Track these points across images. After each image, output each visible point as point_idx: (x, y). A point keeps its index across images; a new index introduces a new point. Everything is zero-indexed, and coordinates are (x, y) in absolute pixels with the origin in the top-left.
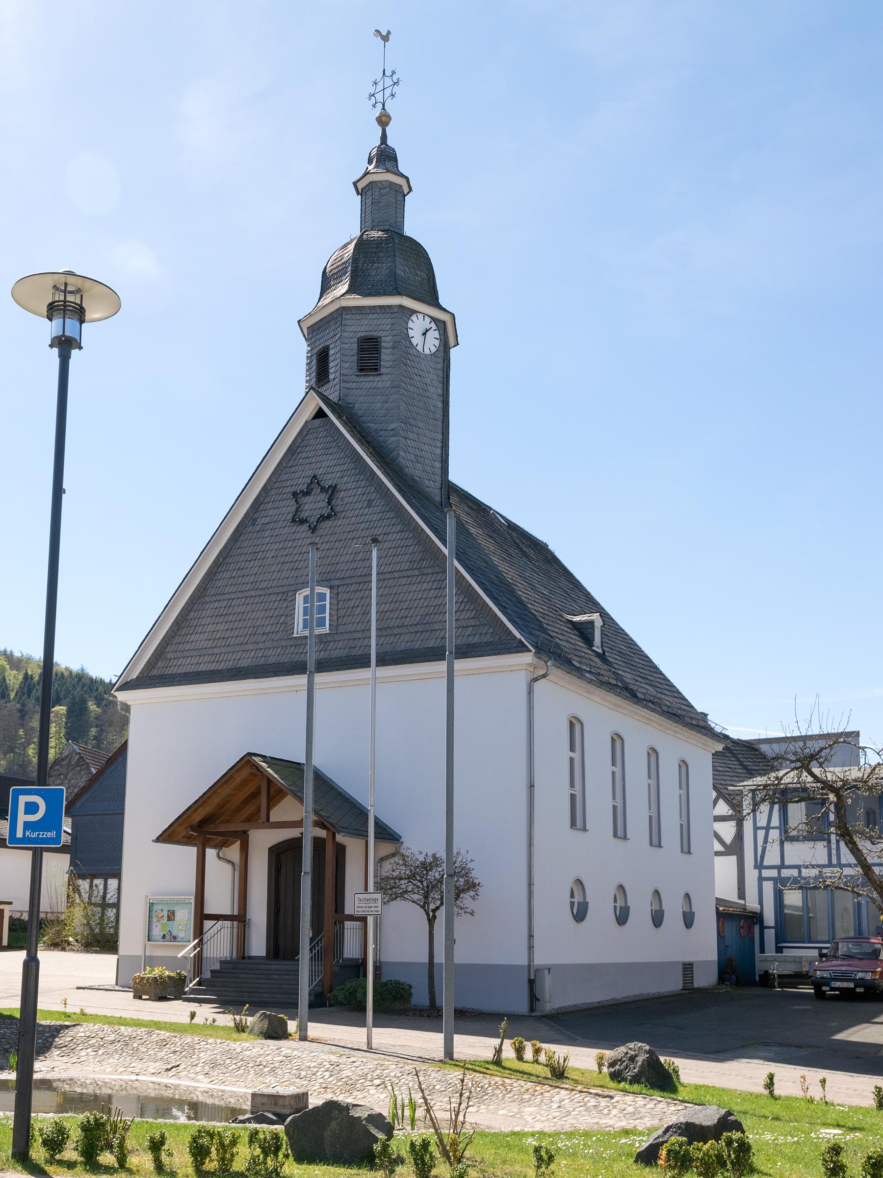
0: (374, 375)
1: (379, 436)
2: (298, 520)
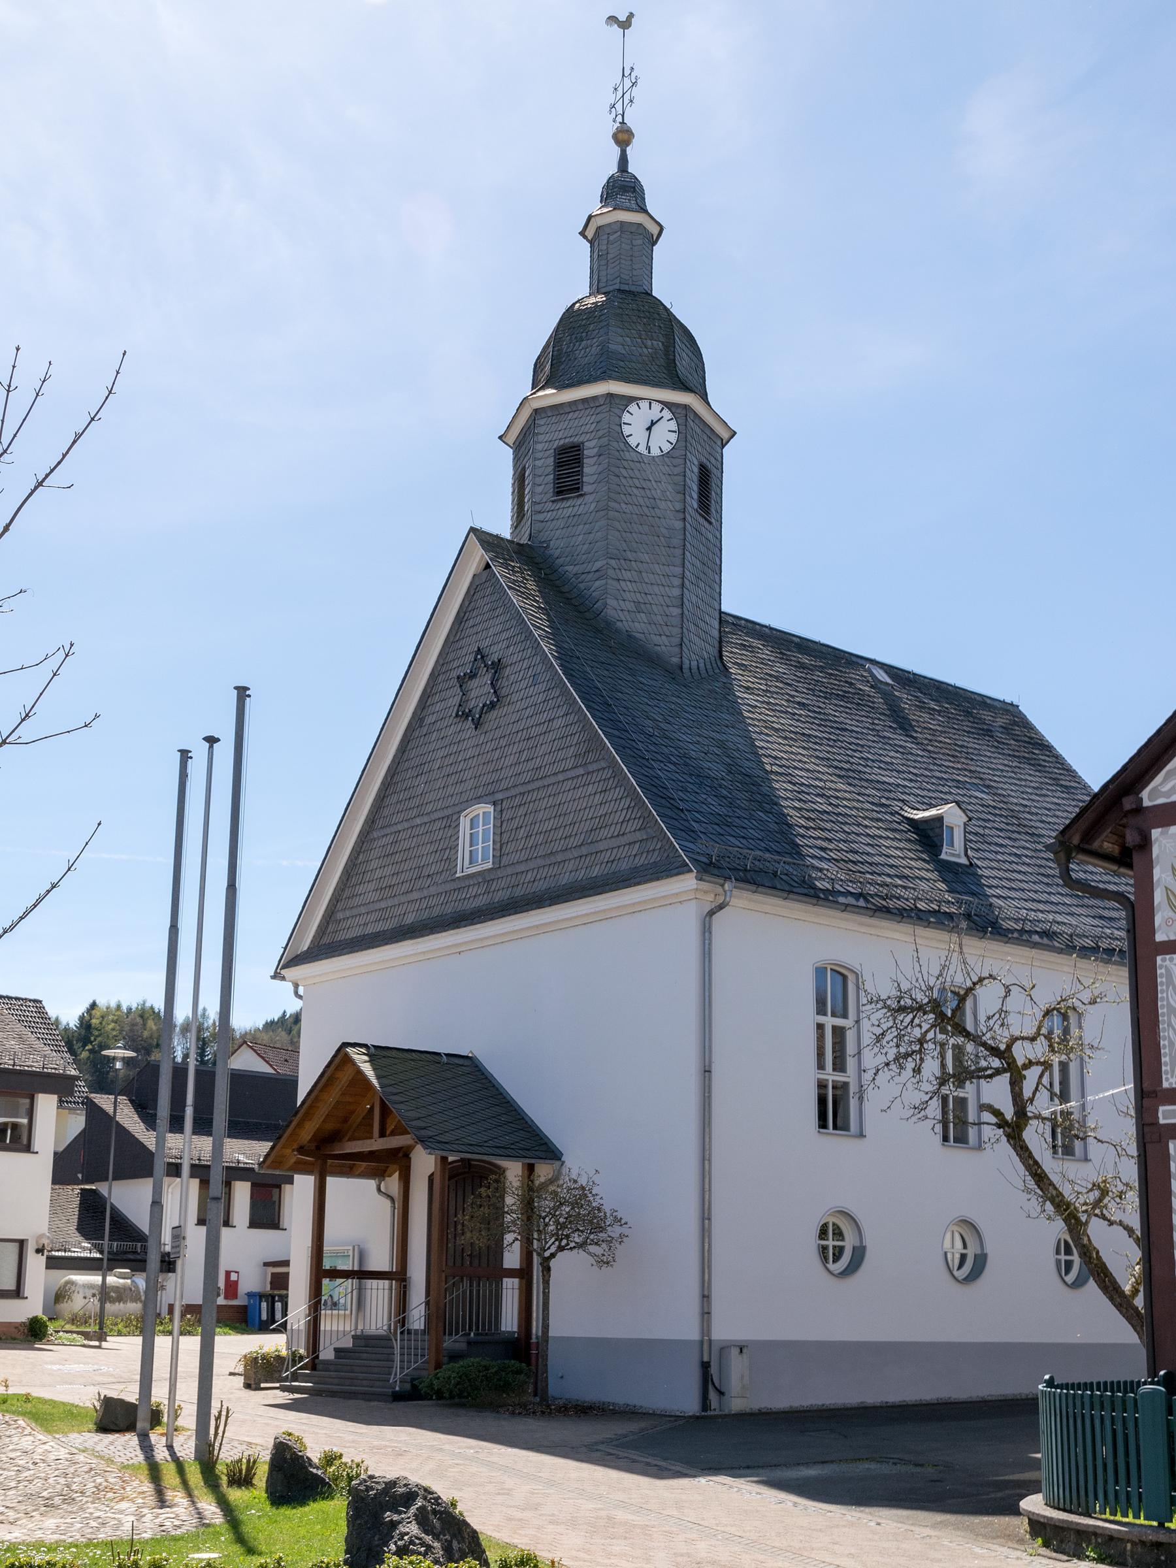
0: (574, 497)
1: (580, 583)
2: (464, 714)
